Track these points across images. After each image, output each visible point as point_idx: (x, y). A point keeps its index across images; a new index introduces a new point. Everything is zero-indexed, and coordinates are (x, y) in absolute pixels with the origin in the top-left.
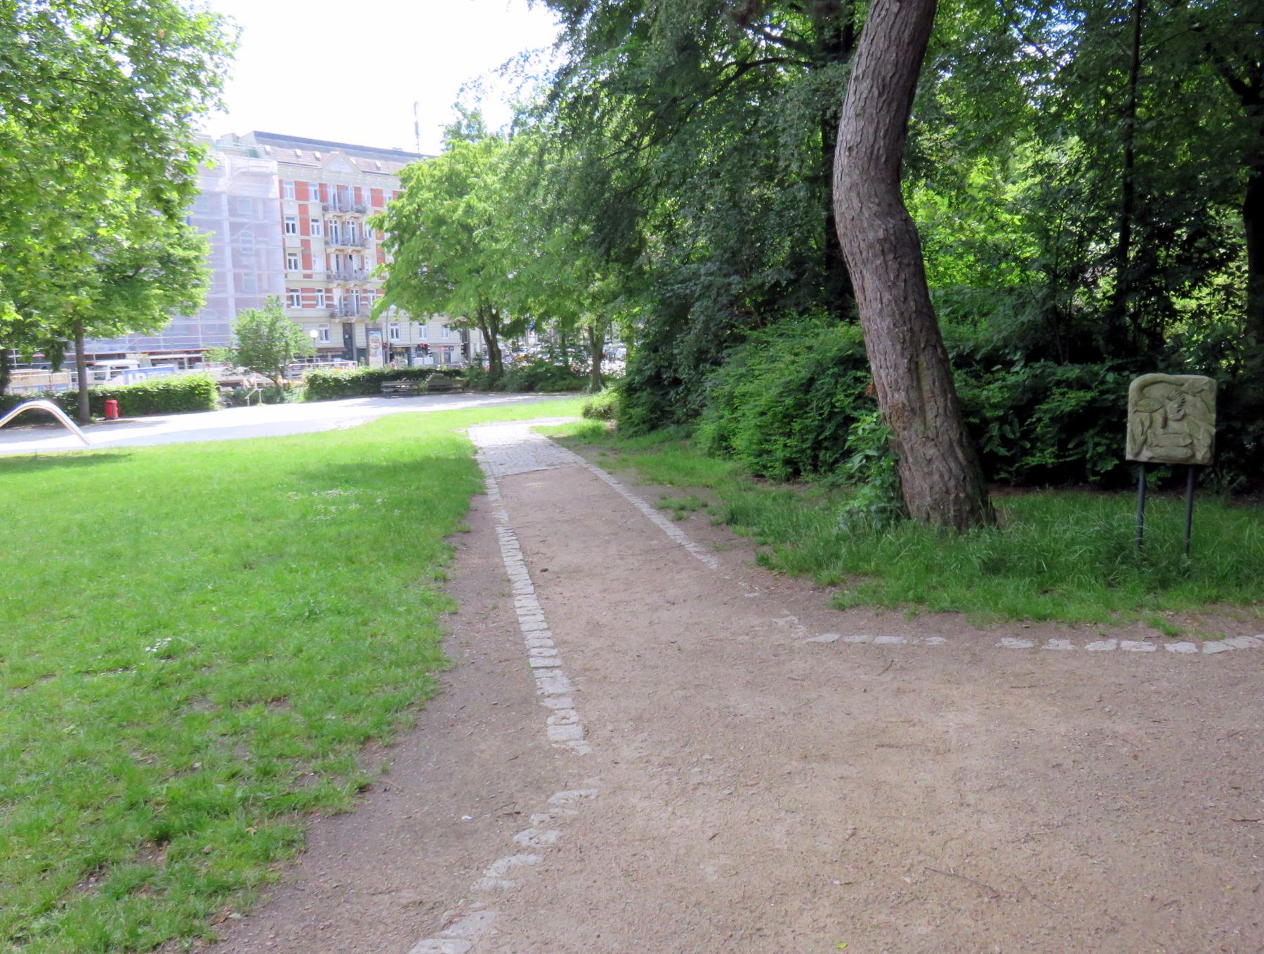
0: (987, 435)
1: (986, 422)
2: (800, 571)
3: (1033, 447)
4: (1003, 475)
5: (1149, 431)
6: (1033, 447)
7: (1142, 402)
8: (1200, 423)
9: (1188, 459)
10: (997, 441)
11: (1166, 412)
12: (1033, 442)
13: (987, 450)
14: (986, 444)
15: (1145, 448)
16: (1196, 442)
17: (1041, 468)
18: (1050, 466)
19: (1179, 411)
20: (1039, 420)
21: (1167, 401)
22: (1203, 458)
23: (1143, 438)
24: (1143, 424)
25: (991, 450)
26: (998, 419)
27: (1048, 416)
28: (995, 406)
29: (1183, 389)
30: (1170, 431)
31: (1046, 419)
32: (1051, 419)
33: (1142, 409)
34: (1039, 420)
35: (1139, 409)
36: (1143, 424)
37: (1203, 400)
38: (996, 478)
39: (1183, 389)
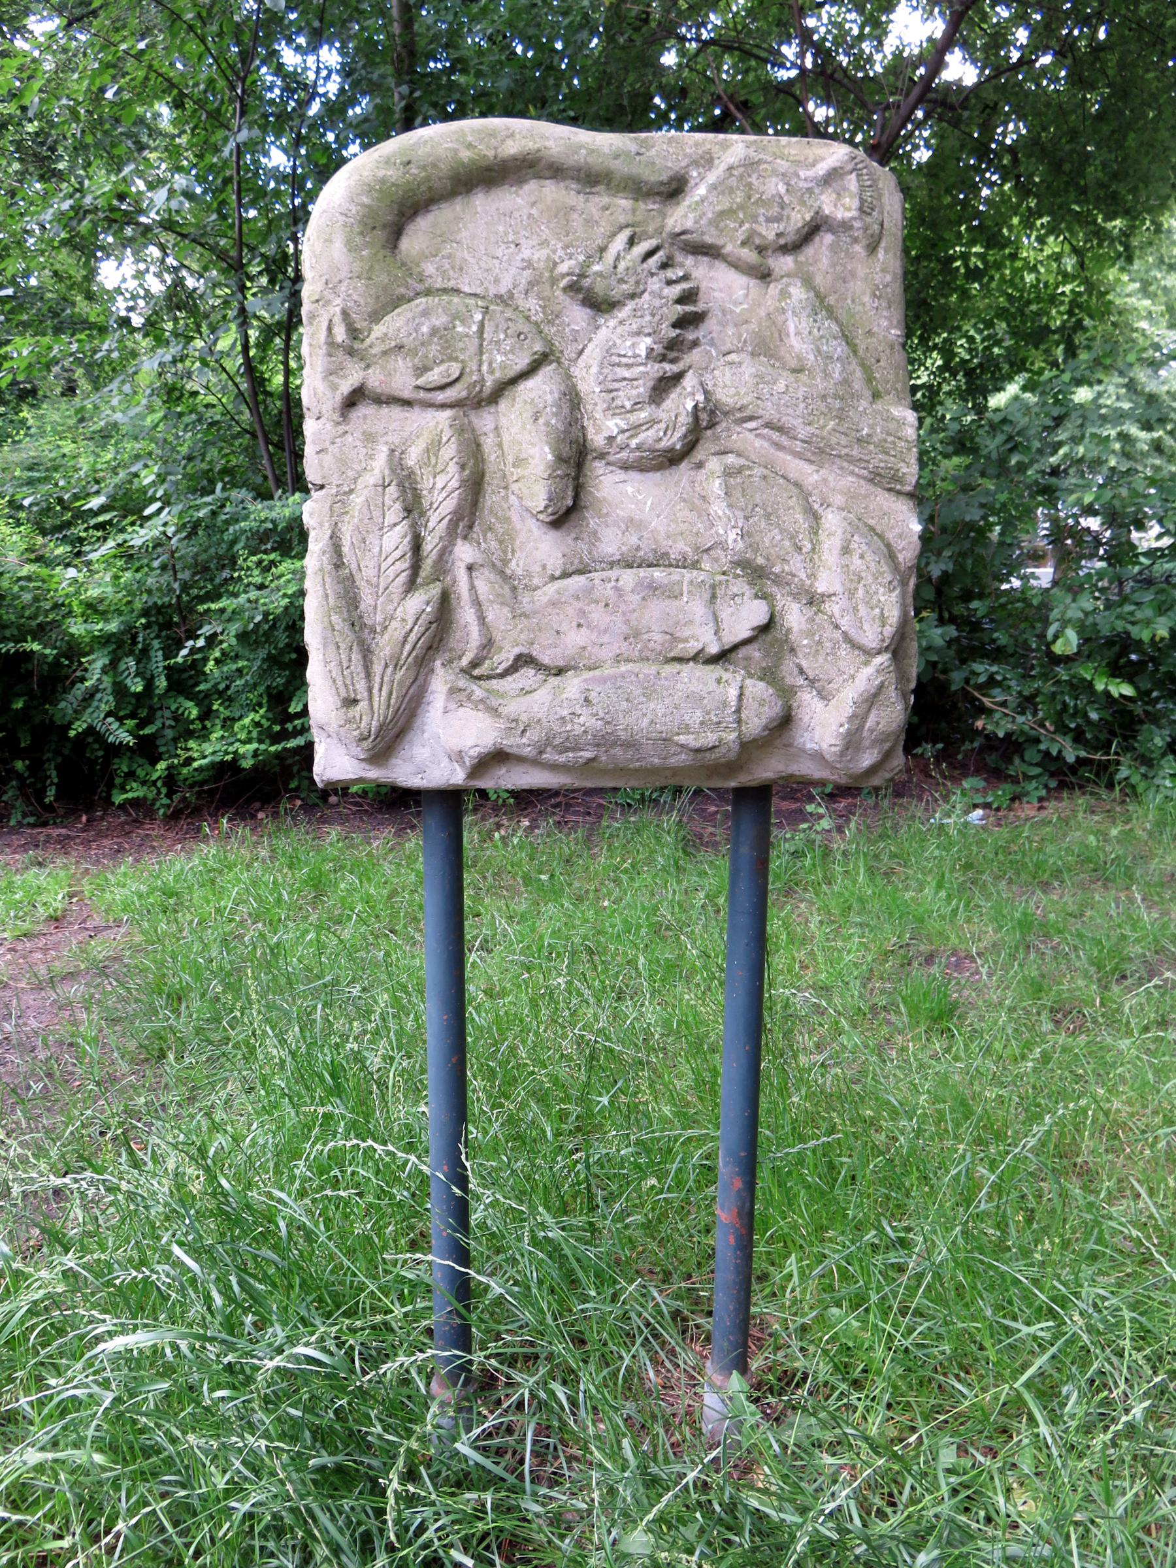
0: (79, 690)
1: (74, 651)
2: (345, 790)
3: (207, 714)
4: (136, 791)
5: (464, 553)
6: (207, 714)
7: (395, 325)
8: (810, 475)
9: (751, 748)
10: (106, 703)
11: (572, 400)
12: (203, 701)
13: (79, 726)
14: (78, 713)
15: (440, 682)
16: (794, 617)
17: (226, 769)
18: (247, 764)
19: (664, 386)
20: (212, 640)
21: (577, 316)
22: (852, 742)
23: (419, 603)
24: (413, 507)
25: (91, 730)
26: (105, 640)
27: (234, 628)
28: (93, 609)
29: (680, 217)
30: (611, 543)
31: (229, 640)
32: (243, 637)
33: (402, 381)
34: (212, 640)
35: (375, 379)
36: (413, 507)
37: (822, 305)
38: (118, 798)
39: (680, 217)
